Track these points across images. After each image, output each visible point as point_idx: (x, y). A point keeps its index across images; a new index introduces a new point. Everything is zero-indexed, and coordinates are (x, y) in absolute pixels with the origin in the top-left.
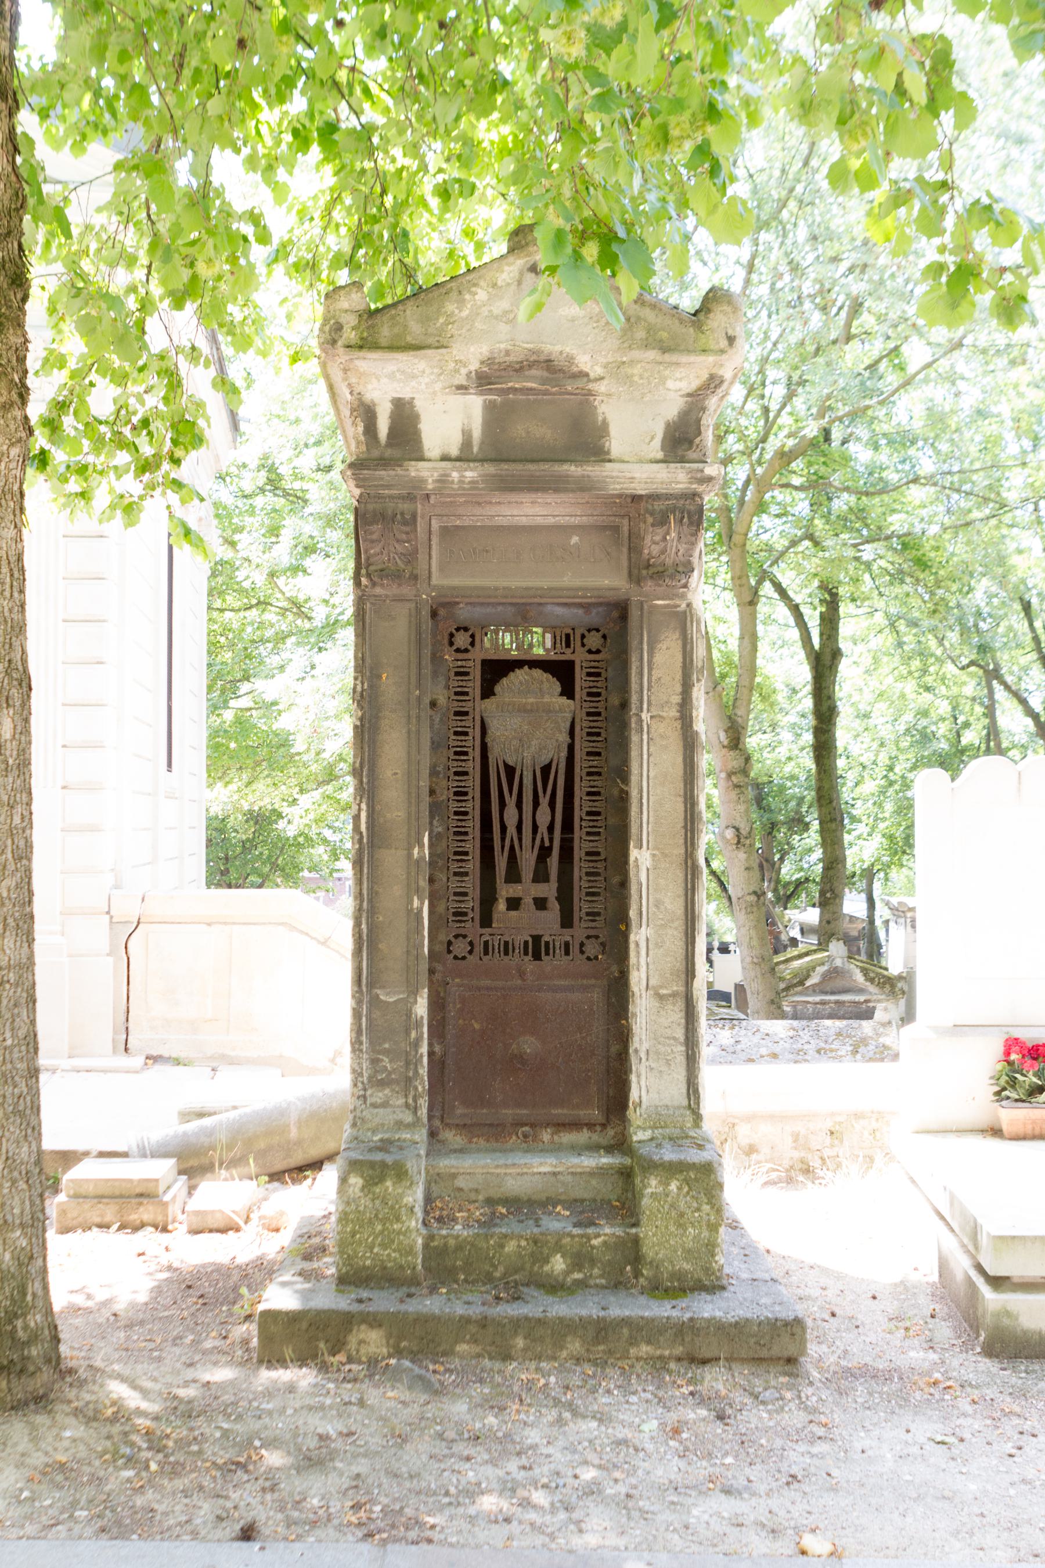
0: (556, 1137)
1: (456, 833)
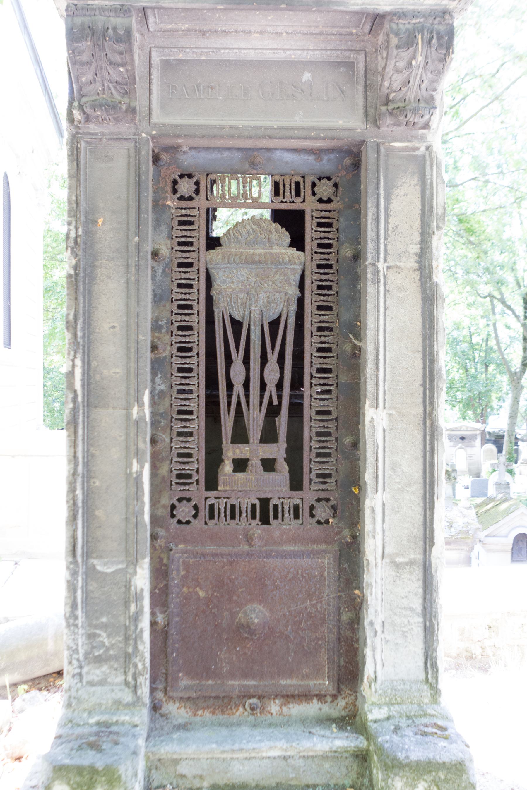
0: (284, 709)
1: (180, 391)
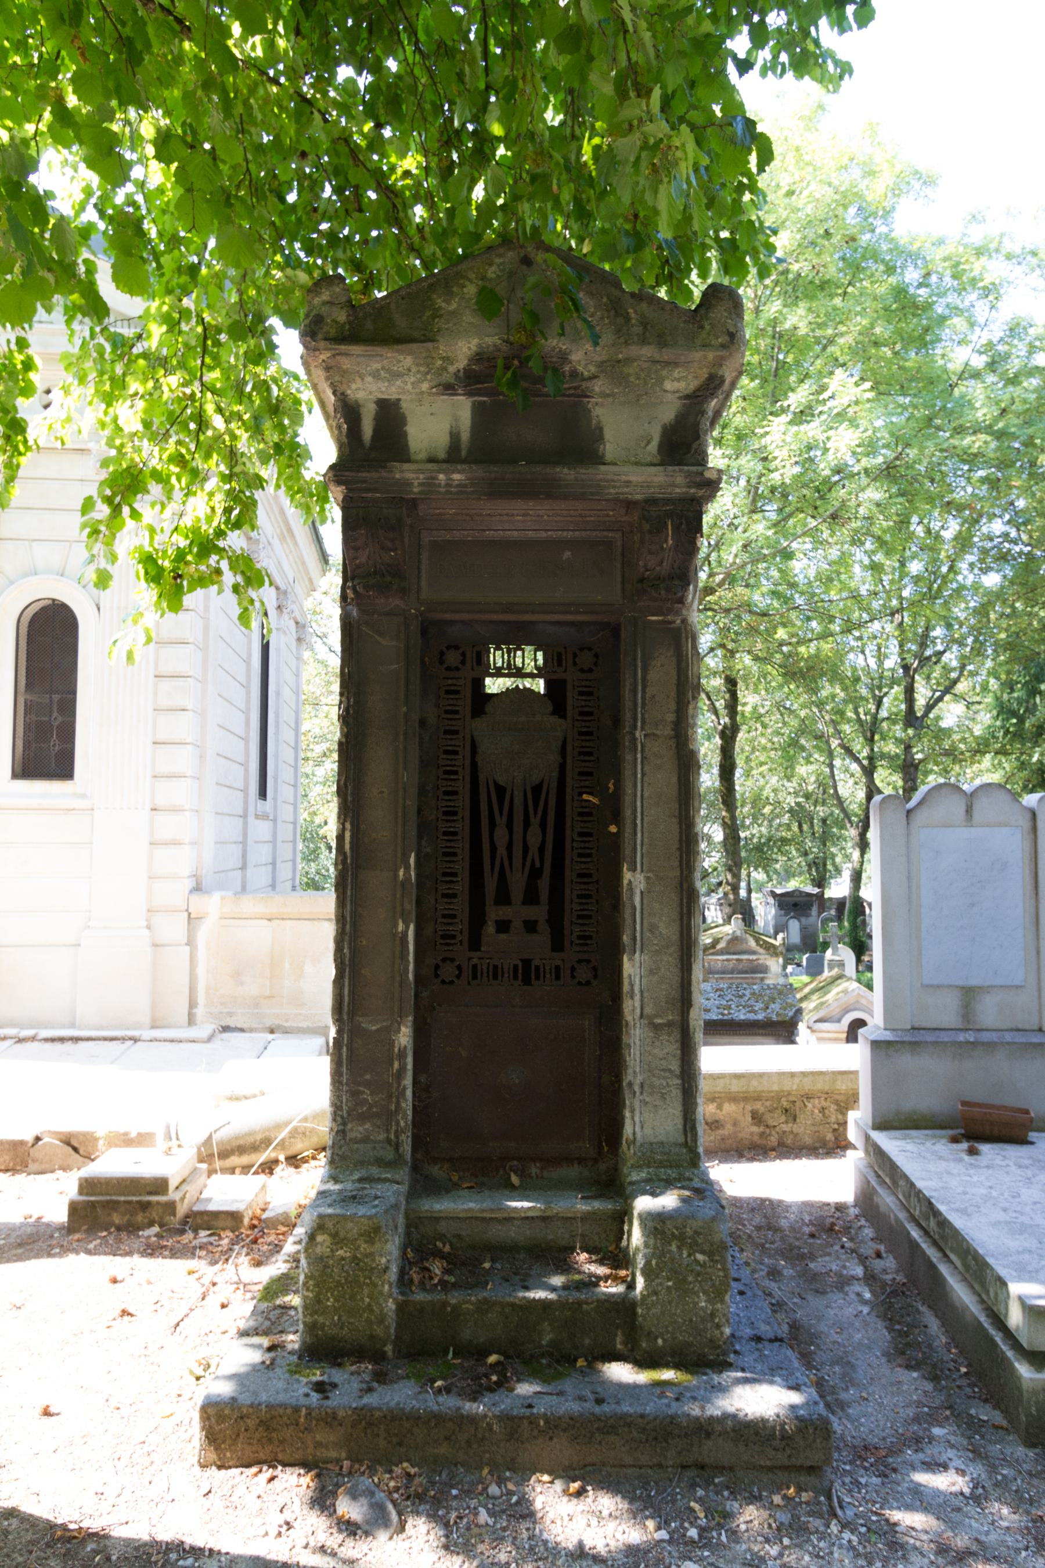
1: (445, 854)
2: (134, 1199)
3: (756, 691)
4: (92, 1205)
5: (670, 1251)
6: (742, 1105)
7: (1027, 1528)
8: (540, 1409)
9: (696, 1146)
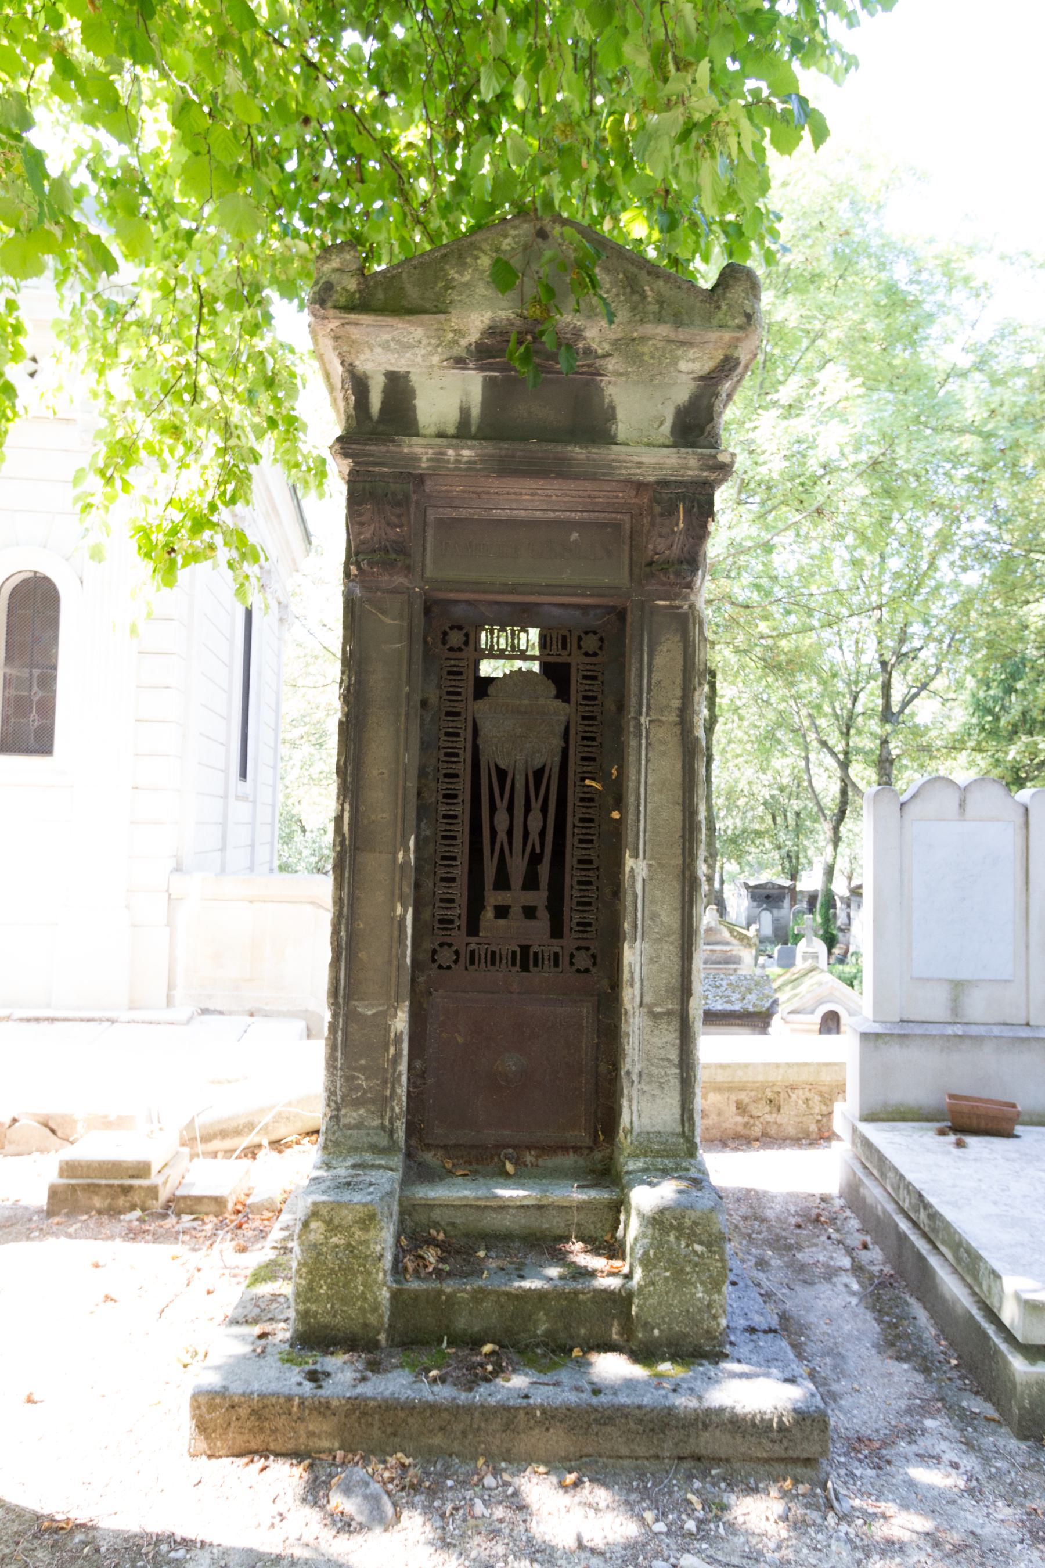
1: (444, 837)
2: (116, 1182)
3: (733, 683)
4: (73, 1188)
5: (668, 1241)
6: (727, 1095)
7: (1022, 1521)
8: (536, 1400)
9: (693, 1136)
